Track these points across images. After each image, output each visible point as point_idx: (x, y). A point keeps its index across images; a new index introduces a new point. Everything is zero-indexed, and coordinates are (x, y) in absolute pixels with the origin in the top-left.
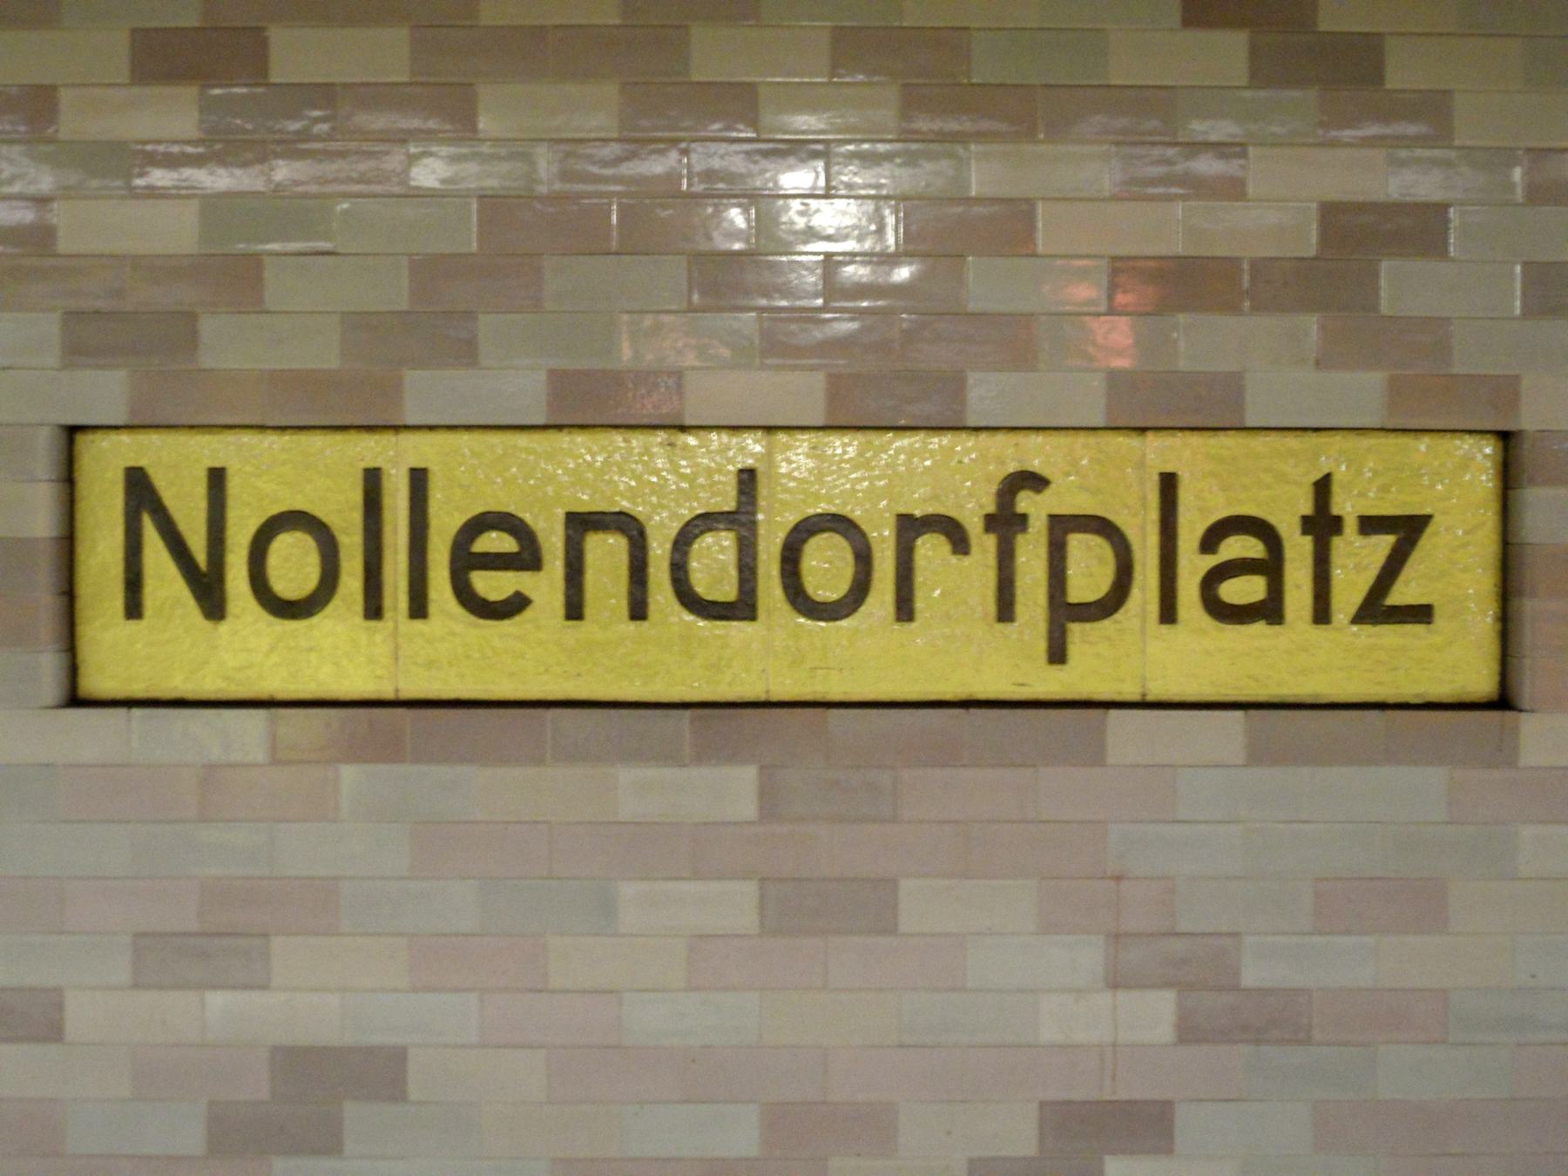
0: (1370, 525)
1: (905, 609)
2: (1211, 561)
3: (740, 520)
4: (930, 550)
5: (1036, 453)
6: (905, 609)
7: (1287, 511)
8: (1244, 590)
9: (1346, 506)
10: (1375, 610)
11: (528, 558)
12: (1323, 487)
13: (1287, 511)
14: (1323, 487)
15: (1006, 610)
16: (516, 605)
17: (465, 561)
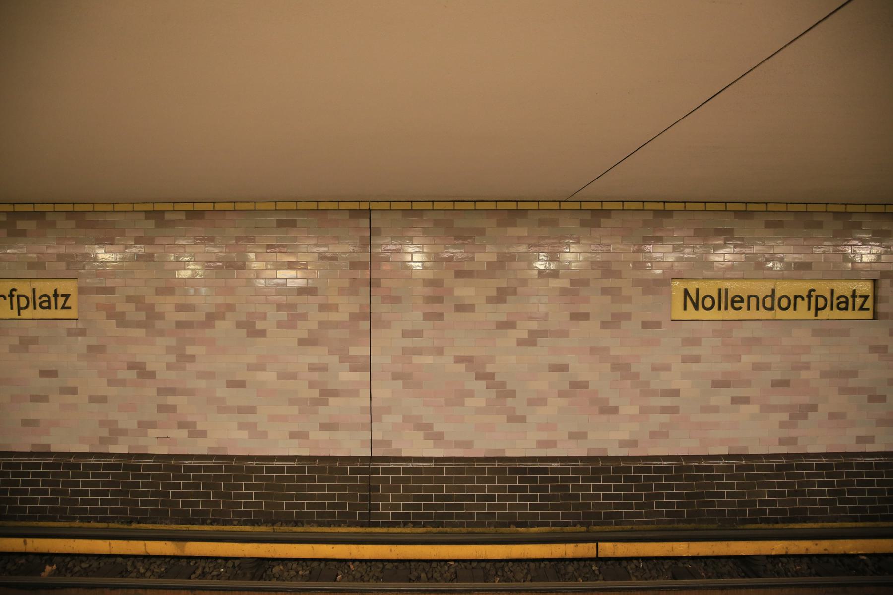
0: (861, 296)
1: (795, 309)
3: (772, 296)
4: (799, 299)
5: (727, 284)
6: (795, 309)
7: (849, 294)
8: (843, 306)
10: (63, 308)
11: (742, 301)
12: (55, 290)
13: (849, 294)
14: (55, 290)
15: (809, 309)
16: (740, 308)
17: (733, 302)
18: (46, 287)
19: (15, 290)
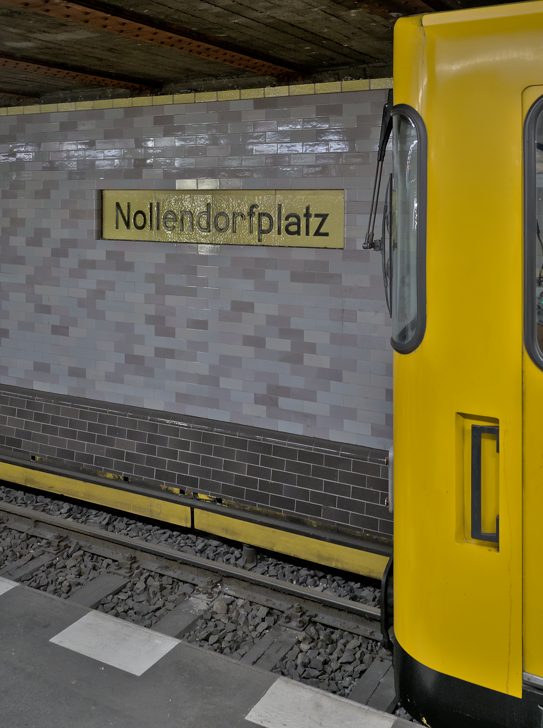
0: (317, 216)
2: (287, 222)
8: (293, 228)
9: (312, 211)
10: (317, 233)
12: (308, 209)
14: (308, 209)
18: (296, 202)
19: (254, 206)
